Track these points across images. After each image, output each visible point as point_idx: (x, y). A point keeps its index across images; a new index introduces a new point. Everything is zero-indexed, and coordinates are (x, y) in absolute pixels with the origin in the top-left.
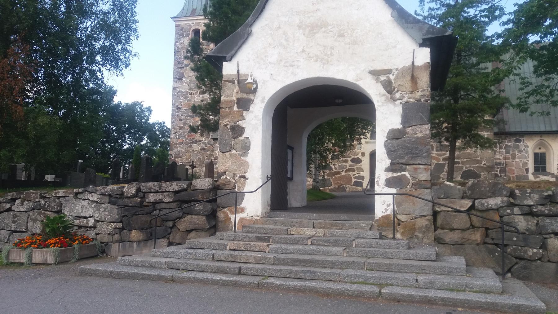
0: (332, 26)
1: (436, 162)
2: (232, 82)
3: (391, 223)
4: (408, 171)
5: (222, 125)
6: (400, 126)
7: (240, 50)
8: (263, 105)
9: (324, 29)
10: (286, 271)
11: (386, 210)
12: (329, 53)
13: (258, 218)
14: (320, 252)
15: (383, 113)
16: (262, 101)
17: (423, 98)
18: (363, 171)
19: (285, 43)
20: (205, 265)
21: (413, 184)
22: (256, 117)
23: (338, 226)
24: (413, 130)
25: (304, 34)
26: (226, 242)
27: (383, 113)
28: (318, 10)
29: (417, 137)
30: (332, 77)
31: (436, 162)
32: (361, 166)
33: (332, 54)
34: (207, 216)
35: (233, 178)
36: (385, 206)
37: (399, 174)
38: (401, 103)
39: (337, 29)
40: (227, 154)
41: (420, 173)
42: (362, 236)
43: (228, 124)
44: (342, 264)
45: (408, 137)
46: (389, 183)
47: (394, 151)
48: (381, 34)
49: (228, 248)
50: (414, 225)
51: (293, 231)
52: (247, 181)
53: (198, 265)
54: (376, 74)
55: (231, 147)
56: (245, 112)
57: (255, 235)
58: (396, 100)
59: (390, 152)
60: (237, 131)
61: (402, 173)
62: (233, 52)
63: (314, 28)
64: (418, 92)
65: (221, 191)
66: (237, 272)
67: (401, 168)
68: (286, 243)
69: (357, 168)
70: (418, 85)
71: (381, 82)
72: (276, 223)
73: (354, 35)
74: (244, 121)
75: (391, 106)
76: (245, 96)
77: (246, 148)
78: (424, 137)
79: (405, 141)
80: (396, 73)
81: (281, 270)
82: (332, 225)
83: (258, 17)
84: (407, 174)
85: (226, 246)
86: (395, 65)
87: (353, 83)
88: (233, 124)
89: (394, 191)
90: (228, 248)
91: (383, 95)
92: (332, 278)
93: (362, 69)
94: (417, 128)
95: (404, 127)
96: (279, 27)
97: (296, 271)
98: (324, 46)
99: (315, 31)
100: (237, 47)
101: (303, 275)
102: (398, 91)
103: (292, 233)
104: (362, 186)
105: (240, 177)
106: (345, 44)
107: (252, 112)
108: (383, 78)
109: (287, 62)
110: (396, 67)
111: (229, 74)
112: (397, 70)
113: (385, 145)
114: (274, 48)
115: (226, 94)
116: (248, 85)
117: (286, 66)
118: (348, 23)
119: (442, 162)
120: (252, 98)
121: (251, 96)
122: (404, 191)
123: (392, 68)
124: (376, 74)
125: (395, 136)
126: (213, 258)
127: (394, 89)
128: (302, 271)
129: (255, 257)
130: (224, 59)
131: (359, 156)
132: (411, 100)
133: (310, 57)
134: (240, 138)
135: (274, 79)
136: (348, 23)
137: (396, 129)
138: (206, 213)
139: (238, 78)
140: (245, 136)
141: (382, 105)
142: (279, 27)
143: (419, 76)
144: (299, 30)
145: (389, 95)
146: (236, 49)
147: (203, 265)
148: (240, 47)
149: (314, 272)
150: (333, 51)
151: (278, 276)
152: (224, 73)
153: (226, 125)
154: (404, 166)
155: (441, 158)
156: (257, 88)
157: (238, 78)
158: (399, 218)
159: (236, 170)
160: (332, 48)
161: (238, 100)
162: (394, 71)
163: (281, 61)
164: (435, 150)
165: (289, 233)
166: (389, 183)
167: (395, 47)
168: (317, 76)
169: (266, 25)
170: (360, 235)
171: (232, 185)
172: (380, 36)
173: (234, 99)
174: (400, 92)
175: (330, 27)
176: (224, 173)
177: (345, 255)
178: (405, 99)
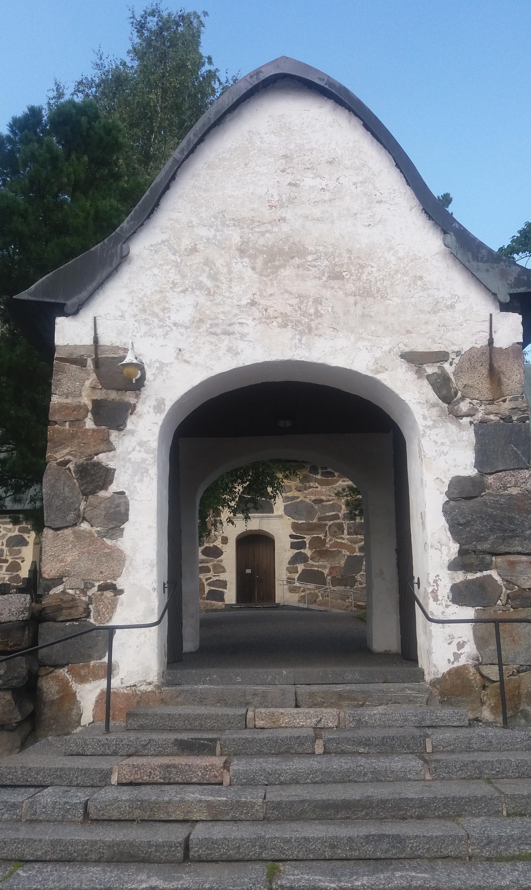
0: (315, 256)
1: (348, 553)
2: (80, 362)
3: (455, 686)
4: (496, 568)
5: (53, 464)
6: (472, 472)
7: (101, 292)
8: (160, 418)
9: (297, 261)
10: (323, 843)
11: (457, 656)
12: (312, 311)
13: (150, 688)
14: (365, 774)
15: (436, 442)
16: (158, 408)
17: (515, 414)
18: (224, 571)
19: (209, 283)
20: (77, 842)
21: (508, 597)
22: (141, 444)
23: (354, 699)
24: (500, 479)
25: (253, 269)
26: (103, 764)
27: (436, 442)
28: (283, 219)
29: (510, 495)
30: (320, 361)
31: (348, 553)
32: (221, 561)
33: (318, 314)
34: (15, 691)
35: (84, 592)
36: (454, 648)
37: (479, 575)
38: (471, 423)
39: (326, 263)
40: (67, 531)
41: (521, 573)
42: (428, 723)
43: (69, 461)
44: (445, 806)
45: (492, 495)
46: (461, 595)
47: (465, 525)
48: (421, 278)
49: (114, 779)
50: (519, 688)
51: (259, 716)
52: (122, 597)
53: (54, 843)
54: (415, 359)
55: (79, 516)
56: (114, 435)
57: (173, 736)
58: (461, 417)
59: (457, 527)
60: (96, 477)
61: (485, 573)
62: (84, 294)
63: (276, 257)
64: (504, 401)
65: (51, 624)
66: (180, 855)
67: (482, 561)
68: (260, 754)
69: (215, 566)
70: (504, 388)
71: (428, 377)
72: (202, 701)
73: (364, 277)
74: (111, 454)
75: (452, 428)
76: (113, 395)
77: (117, 516)
78: (523, 495)
79: (485, 504)
80: (456, 361)
81: (306, 839)
82: (340, 696)
83: (142, 224)
84: (494, 574)
85: (106, 775)
86: (453, 344)
87: (366, 376)
88: (82, 461)
89: (469, 613)
90: (114, 779)
91: (433, 405)
92: (450, 851)
93: (386, 348)
94: (508, 477)
95: (482, 474)
96: (194, 250)
97: (350, 839)
98: (299, 296)
99: (277, 263)
100: (94, 284)
101: (369, 850)
102: (463, 398)
103: (260, 723)
104: (222, 599)
105: (103, 588)
106: (346, 295)
107: (132, 433)
108: (430, 369)
109: (217, 325)
110: (456, 349)
111: (71, 344)
112: (458, 353)
113: (445, 512)
114: (184, 292)
115: (64, 389)
116: (126, 371)
117: (215, 334)
118: (350, 251)
119: (358, 554)
120: (132, 401)
121: (129, 398)
122: (490, 613)
123: (449, 350)
124: (415, 359)
125: (462, 493)
126: (86, 813)
127: (456, 394)
128: (367, 837)
129: (210, 805)
130: (61, 310)
131: (218, 543)
132: (492, 417)
133: (268, 318)
134: (102, 494)
135: (186, 361)
136: (350, 251)
137: (465, 478)
138: (14, 683)
139: (96, 354)
140: (114, 488)
141: (434, 426)
142: (194, 250)
143: (504, 368)
144: (242, 257)
145: (446, 405)
146: (90, 288)
147: (72, 843)
148: (101, 285)
149: (398, 839)
150: (320, 308)
151: (301, 856)
152: (60, 340)
153: (65, 463)
154: (488, 557)
155: (357, 546)
156: (143, 378)
157: (96, 354)
158: (485, 673)
159: (90, 571)
160: (318, 301)
161: (96, 403)
162: (452, 356)
163: (201, 321)
164: (346, 532)
165: (250, 724)
166: (461, 595)
167: (452, 307)
168: (286, 358)
169: (163, 242)
170: (423, 719)
171: (81, 609)
172: (419, 283)
173: (86, 401)
174: (468, 400)
175: (310, 258)
176: (58, 581)
177: (428, 777)
178: (480, 415)
